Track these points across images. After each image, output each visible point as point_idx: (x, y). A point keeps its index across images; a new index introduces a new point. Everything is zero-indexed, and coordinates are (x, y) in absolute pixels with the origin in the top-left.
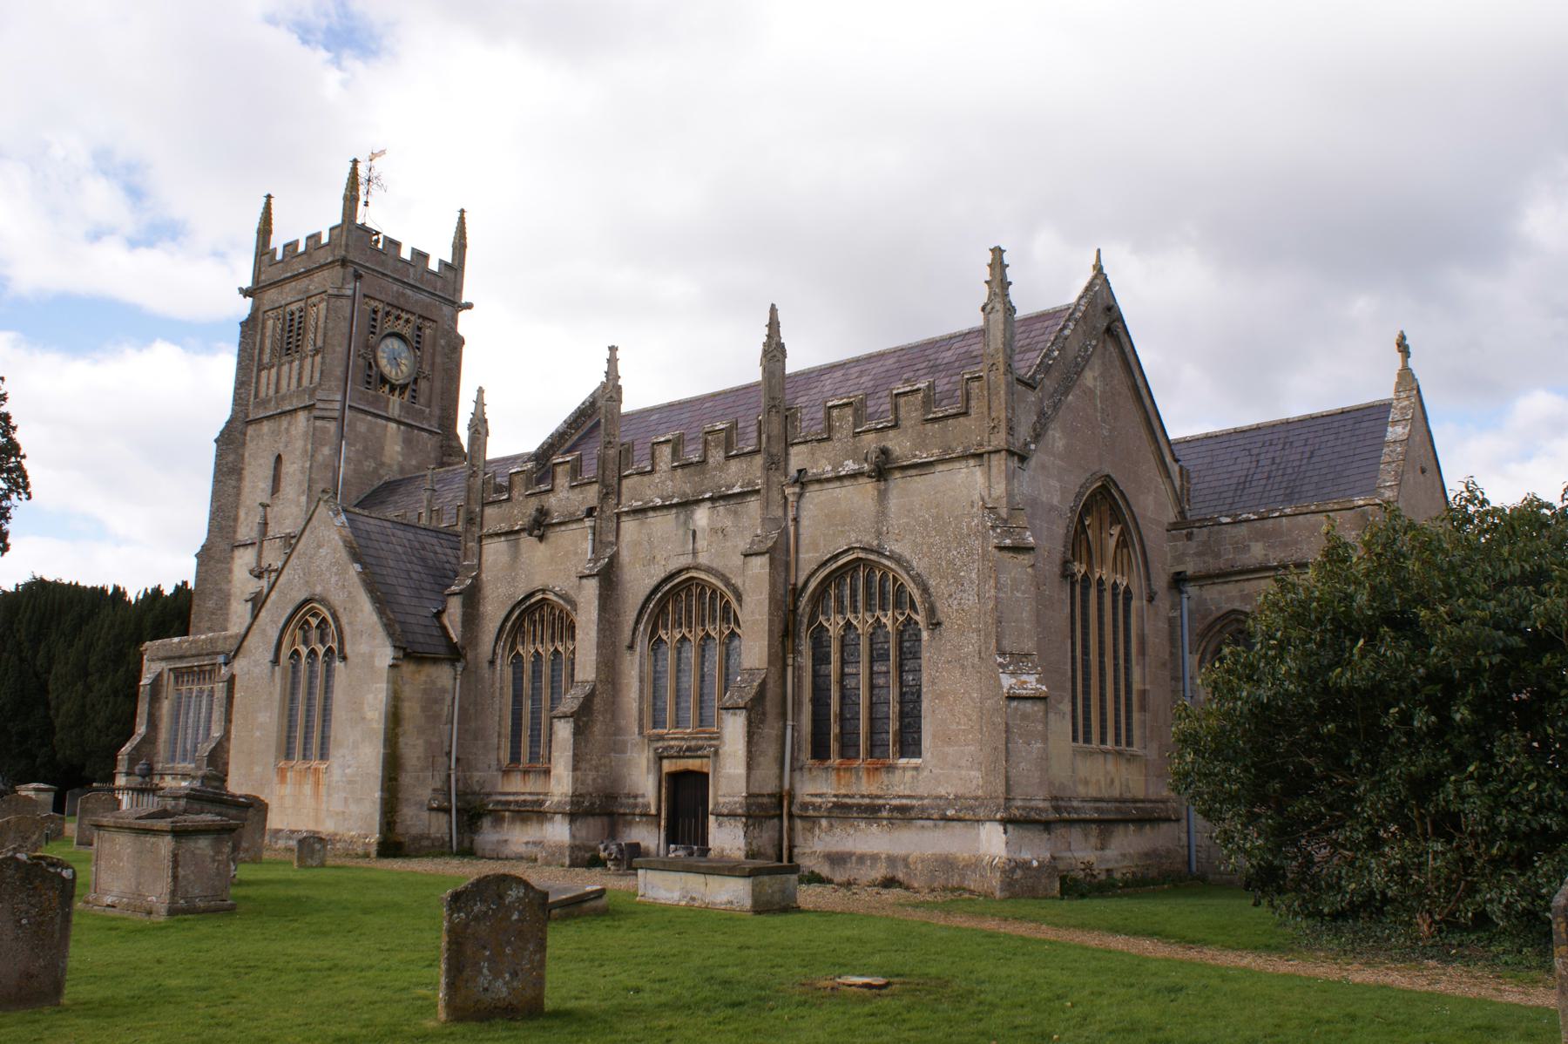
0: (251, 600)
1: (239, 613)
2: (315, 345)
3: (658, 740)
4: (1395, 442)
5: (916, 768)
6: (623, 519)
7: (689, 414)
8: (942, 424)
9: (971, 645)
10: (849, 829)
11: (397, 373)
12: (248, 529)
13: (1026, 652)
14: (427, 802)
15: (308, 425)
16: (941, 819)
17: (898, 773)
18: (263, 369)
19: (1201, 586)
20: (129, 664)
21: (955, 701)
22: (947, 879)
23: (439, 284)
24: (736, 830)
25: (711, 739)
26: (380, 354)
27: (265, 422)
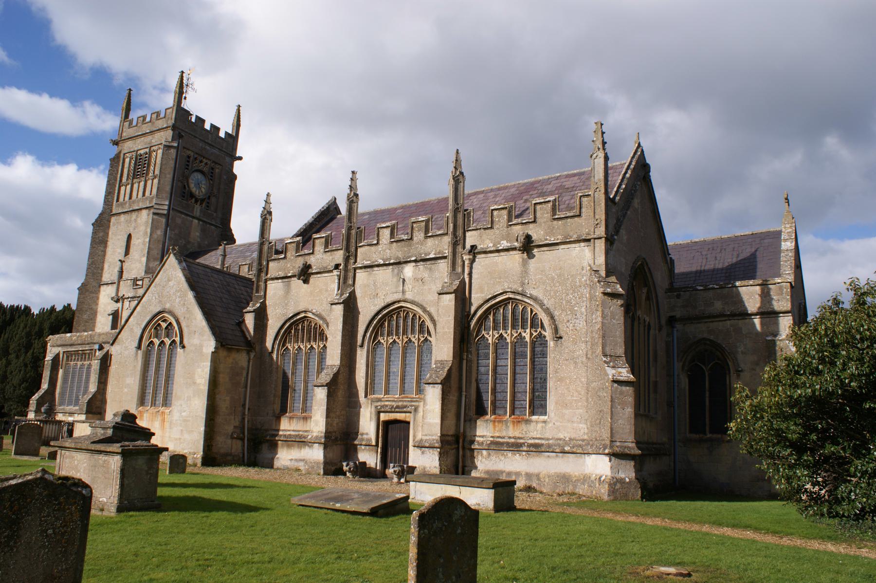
0: (112, 314)
1: (103, 324)
2: (154, 173)
3: (377, 401)
4: (787, 250)
5: (545, 422)
6: (358, 271)
7: (388, 216)
8: (563, 221)
9: (581, 350)
10: (500, 457)
11: (199, 193)
12: (110, 275)
13: (618, 355)
14: (230, 434)
15: (148, 218)
16: (561, 452)
17: (532, 424)
18: (123, 185)
19: (684, 325)
20: (34, 349)
21: (570, 383)
22: (564, 488)
23: (225, 145)
24: (433, 456)
25: (412, 401)
26: (190, 181)
27: (122, 215)
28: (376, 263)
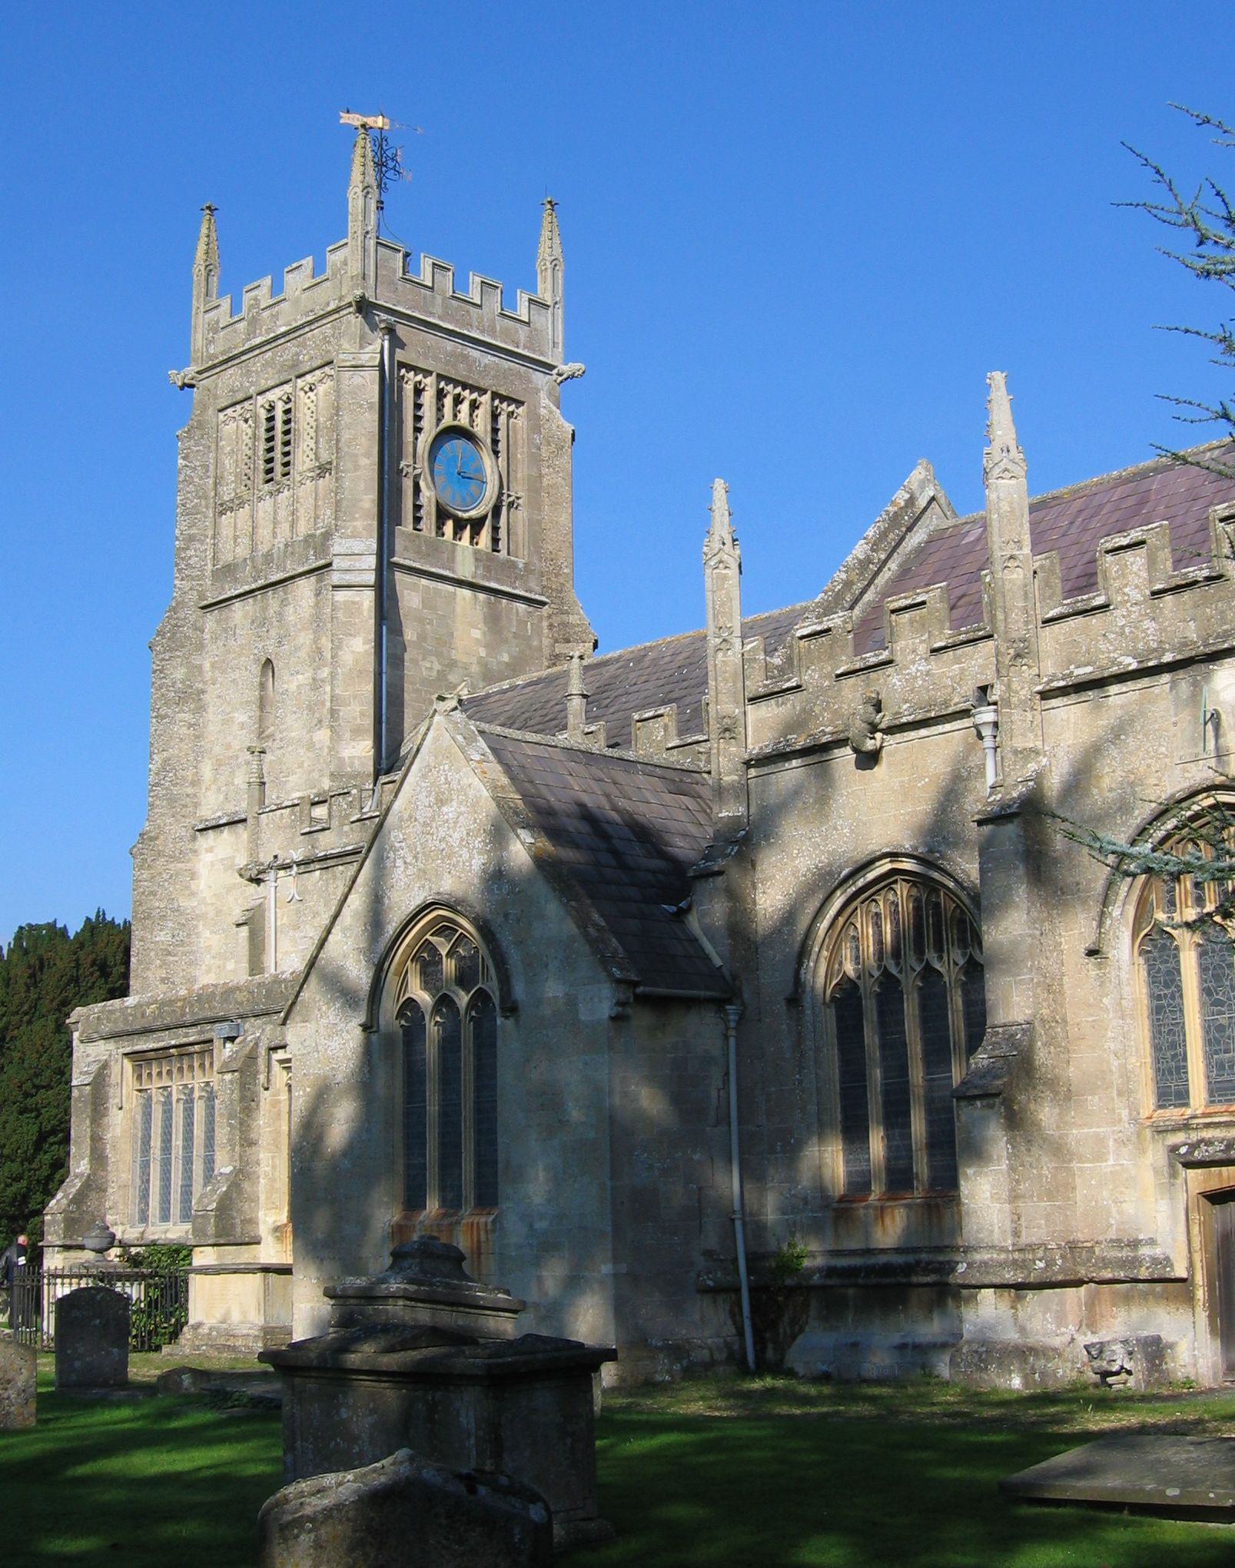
12: (221, 798)
27: (237, 605)
28: (1115, 670)
